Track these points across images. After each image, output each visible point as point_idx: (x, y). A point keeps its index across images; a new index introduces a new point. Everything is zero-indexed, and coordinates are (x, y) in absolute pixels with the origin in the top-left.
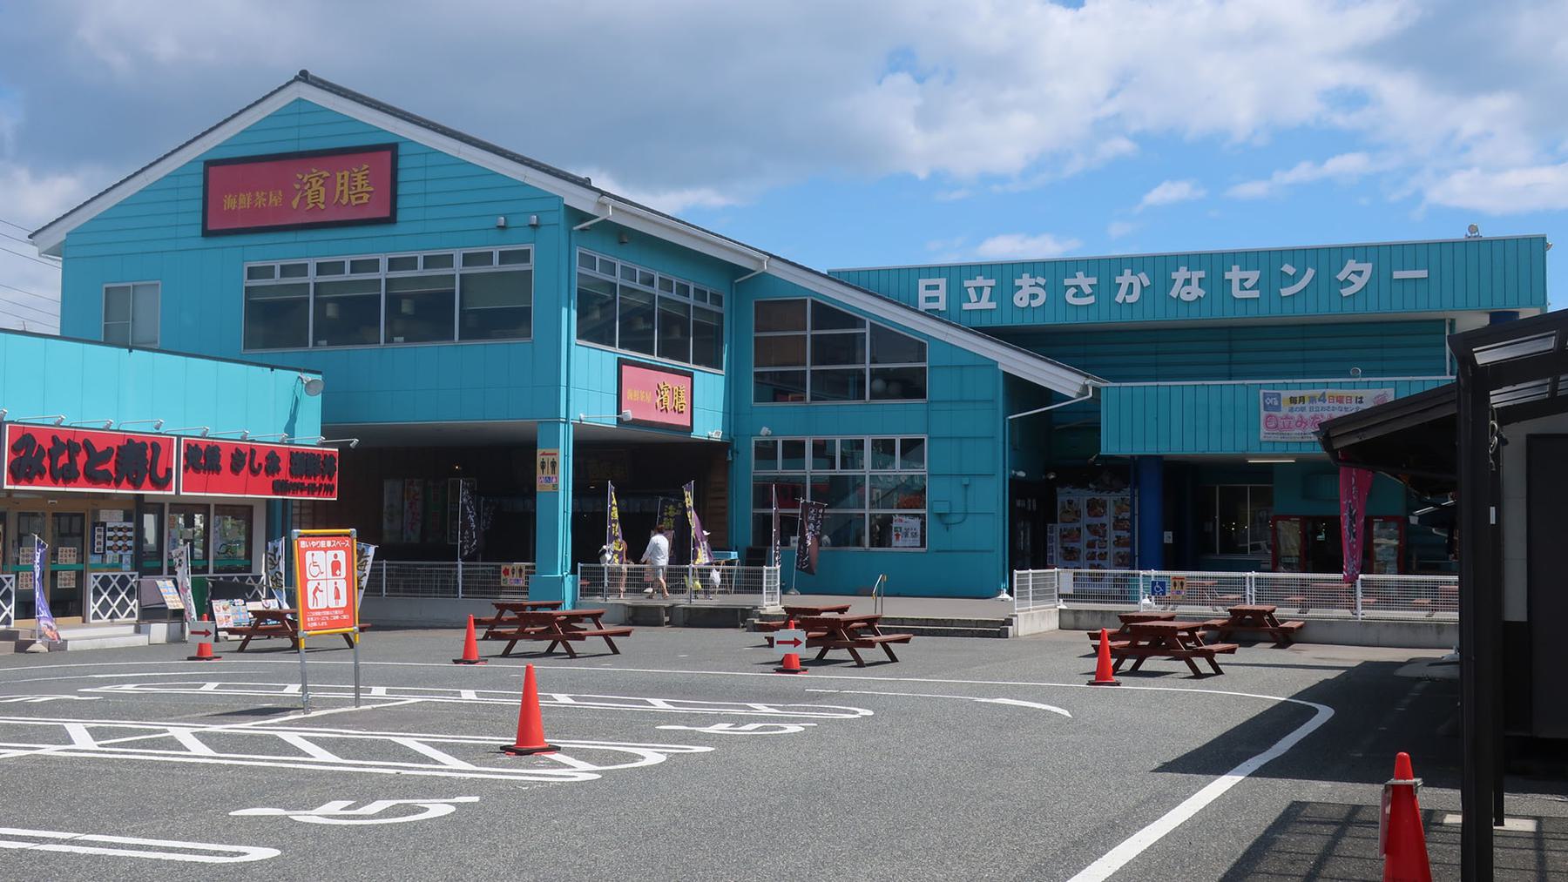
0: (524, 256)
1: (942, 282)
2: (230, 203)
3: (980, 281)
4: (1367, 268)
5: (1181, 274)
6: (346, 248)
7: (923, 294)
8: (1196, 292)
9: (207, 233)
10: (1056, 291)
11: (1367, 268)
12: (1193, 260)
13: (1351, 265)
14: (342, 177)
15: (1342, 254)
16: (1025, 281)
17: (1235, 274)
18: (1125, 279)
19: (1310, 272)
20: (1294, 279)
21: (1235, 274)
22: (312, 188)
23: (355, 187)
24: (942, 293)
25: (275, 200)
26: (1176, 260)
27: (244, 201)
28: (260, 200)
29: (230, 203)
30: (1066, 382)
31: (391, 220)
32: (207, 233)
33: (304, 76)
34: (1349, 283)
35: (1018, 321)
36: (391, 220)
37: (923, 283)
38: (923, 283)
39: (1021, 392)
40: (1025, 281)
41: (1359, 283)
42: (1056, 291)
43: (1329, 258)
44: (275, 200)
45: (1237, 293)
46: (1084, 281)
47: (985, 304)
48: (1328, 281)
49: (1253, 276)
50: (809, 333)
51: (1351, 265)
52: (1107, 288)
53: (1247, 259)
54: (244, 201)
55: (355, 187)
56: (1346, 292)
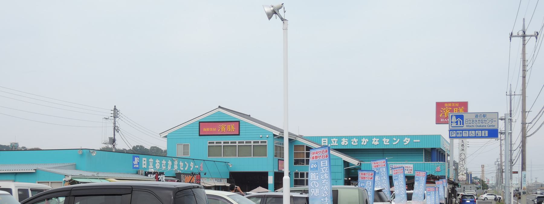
0: (265, 142)
1: (327, 139)
2: (205, 130)
3: (334, 139)
4: (409, 139)
5: (374, 139)
6: (230, 139)
7: (323, 141)
8: (377, 143)
9: (200, 135)
10: (350, 141)
11: (409, 139)
12: (376, 137)
13: (406, 139)
14: (229, 126)
15: (405, 136)
16: (344, 140)
17: (384, 140)
18: (363, 140)
19: (399, 140)
20: (396, 141)
21: (384, 140)
22: (223, 128)
23: (232, 128)
24: (327, 142)
25: (215, 130)
26: (373, 137)
27: (208, 130)
28: (211, 129)
29: (205, 130)
30: (354, 162)
31: (239, 135)
32: (200, 135)
33: (220, 107)
34: (405, 142)
35: (342, 148)
36: (239, 135)
37: (323, 139)
38: (323, 139)
39: (346, 164)
40: (344, 140)
41: (407, 142)
42: (350, 141)
43: (402, 137)
44: (215, 130)
45: (385, 143)
46: (356, 140)
47: (336, 144)
48: (401, 141)
49: (388, 140)
50: (305, 152)
51: (406, 139)
52: (360, 141)
53: (387, 137)
54: (208, 130)
55: (232, 128)
56: (405, 144)
